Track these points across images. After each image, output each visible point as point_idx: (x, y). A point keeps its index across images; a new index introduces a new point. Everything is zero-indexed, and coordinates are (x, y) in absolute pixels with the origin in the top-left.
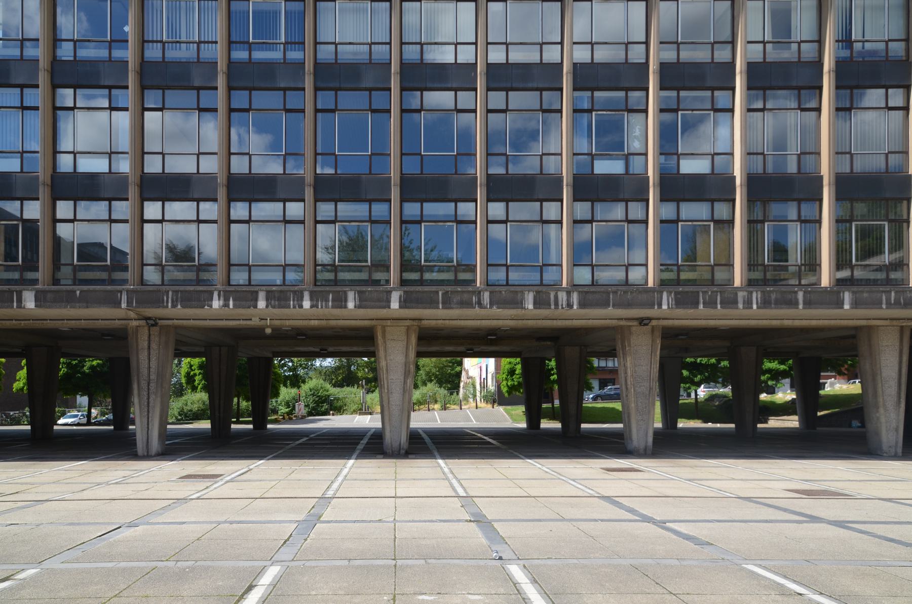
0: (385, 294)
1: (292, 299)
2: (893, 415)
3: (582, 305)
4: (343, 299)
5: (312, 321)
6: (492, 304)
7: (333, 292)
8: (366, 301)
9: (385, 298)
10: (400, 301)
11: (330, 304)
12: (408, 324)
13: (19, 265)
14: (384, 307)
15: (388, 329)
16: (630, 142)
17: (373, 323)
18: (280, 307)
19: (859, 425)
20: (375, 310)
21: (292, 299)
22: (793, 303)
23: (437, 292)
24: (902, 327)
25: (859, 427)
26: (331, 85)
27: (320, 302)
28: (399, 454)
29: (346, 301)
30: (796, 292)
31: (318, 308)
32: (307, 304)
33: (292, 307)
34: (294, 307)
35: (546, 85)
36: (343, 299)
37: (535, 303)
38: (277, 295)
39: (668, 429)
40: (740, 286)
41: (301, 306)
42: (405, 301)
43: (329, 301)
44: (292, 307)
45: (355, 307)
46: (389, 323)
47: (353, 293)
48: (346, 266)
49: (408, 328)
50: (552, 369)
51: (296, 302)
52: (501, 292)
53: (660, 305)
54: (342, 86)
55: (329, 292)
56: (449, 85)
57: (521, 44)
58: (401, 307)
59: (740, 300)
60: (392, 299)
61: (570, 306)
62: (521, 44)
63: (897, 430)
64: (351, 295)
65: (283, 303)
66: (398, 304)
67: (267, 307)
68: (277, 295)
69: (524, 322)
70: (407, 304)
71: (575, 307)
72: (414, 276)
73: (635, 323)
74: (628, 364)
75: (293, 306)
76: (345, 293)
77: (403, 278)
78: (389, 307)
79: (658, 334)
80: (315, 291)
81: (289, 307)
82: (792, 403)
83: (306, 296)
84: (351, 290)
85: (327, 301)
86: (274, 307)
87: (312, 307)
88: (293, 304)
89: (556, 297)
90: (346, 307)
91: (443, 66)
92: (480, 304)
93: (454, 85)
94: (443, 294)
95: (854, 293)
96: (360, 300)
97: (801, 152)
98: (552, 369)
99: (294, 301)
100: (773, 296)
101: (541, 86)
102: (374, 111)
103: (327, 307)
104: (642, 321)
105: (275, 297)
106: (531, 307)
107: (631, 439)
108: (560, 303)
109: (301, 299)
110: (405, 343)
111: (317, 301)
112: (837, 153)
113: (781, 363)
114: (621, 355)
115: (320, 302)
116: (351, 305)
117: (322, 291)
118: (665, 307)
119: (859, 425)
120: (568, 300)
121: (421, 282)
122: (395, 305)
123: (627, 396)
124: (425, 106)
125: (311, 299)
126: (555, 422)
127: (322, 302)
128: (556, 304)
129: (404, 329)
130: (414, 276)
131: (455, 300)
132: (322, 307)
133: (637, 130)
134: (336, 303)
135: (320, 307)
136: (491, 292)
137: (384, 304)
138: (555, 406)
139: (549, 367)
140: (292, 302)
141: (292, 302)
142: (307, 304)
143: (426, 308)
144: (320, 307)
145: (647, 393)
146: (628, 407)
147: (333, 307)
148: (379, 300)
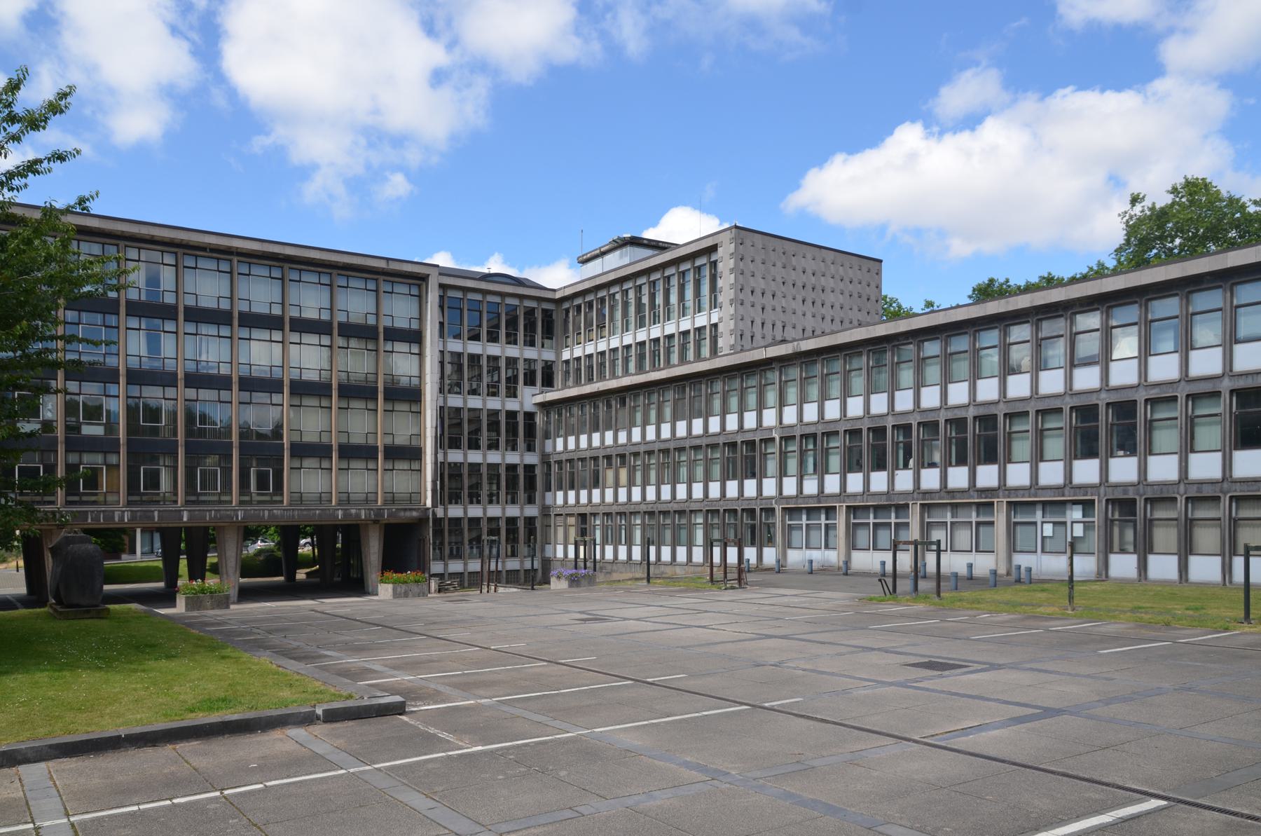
16: (45, 413)
30: (153, 511)
72: (193, 498)
73: (55, 527)
95: (189, 511)
100: (139, 514)
121: (198, 502)
130: (193, 498)
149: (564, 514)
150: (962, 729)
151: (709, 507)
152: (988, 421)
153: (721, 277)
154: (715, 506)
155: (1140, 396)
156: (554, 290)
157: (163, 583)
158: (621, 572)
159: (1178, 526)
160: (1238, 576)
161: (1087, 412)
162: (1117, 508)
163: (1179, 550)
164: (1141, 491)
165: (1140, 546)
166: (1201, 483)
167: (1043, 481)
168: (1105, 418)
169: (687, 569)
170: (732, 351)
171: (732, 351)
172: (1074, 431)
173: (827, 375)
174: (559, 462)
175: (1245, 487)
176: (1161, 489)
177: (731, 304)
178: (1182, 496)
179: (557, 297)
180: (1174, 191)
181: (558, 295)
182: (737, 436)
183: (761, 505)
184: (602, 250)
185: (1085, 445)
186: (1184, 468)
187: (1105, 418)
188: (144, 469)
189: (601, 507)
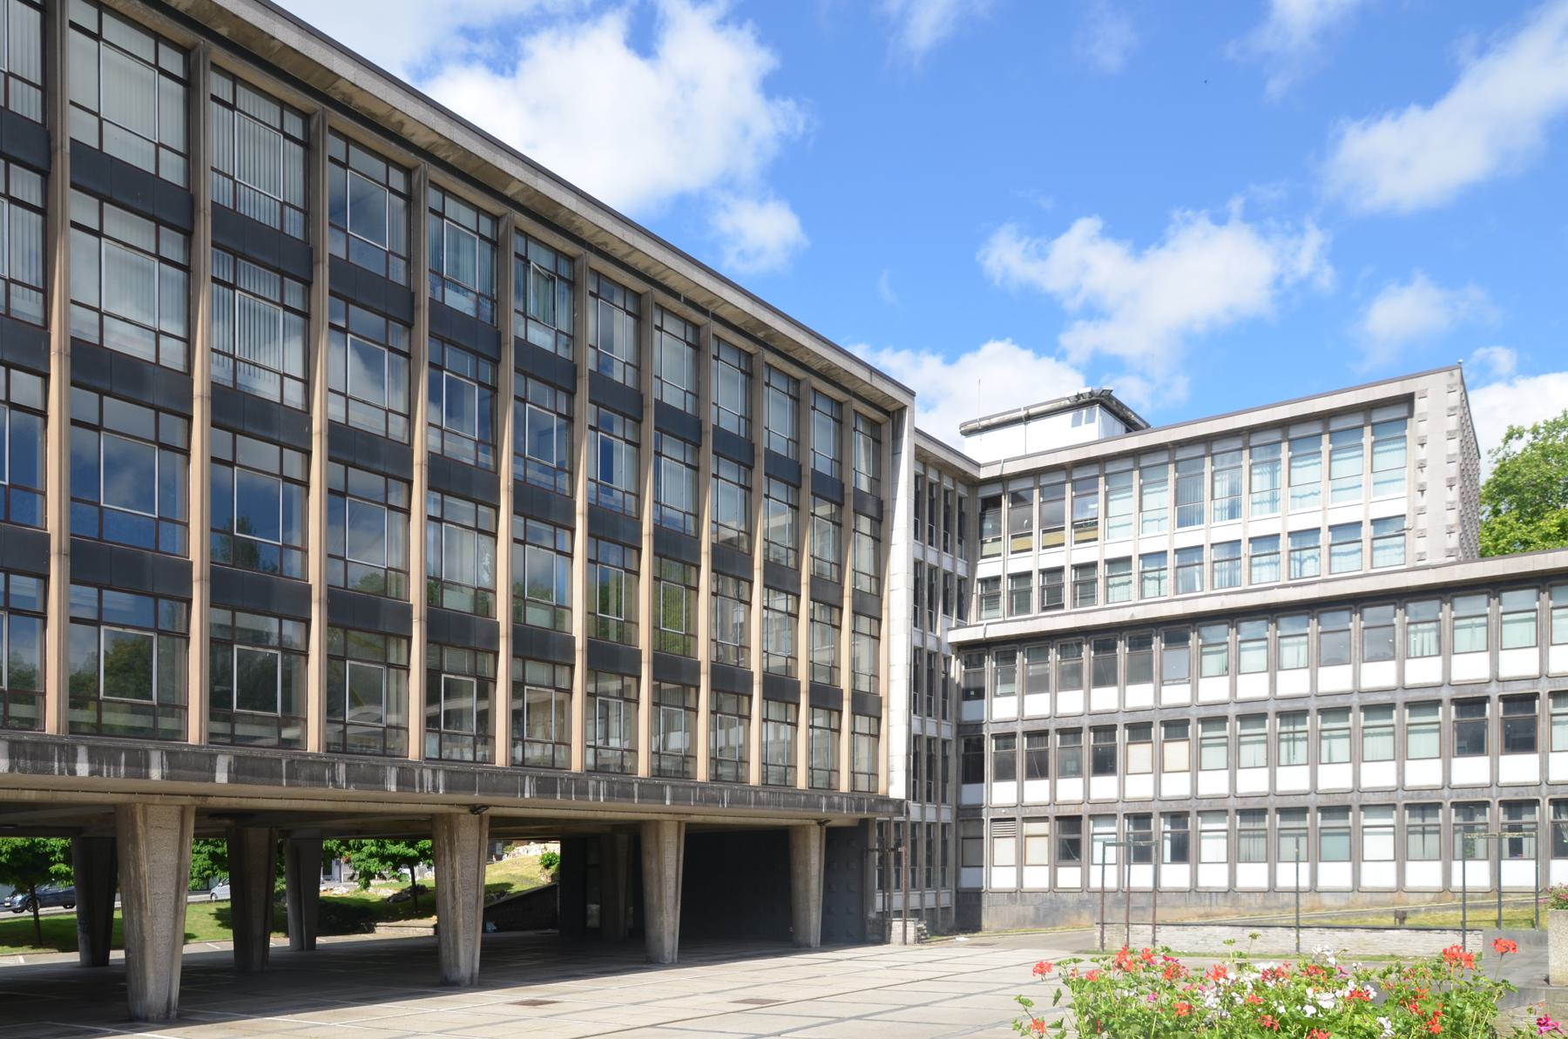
0: (207, 758)
1: (56, 757)
2: (672, 919)
3: (449, 788)
4: (143, 763)
5: (26, 792)
6: (348, 781)
7: (128, 750)
8: (179, 768)
9: (207, 766)
10: (229, 772)
11: (123, 770)
12: (184, 803)
13: (277, 718)
14: (206, 780)
15: (151, 809)
17: (133, 798)
18: (36, 771)
19: (495, 928)
20: (194, 784)
21: (56, 757)
22: (630, 796)
23: (280, 761)
24: (679, 822)
25: (495, 931)
26: (97, 384)
27: (105, 767)
28: (168, 1017)
29: (148, 766)
31: (102, 776)
32: (83, 769)
33: (56, 772)
34: (61, 773)
35: (395, 473)
36: (143, 763)
37: (398, 784)
38: (29, 749)
39: (303, 949)
40: (197, 743)
41: (73, 772)
42: (237, 771)
43: (120, 765)
44: (56, 772)
45: (163, 777)
46: (157, 799)
47: (159, 753)
48: (117, 702)
49: (183, 810)
50: (53, 853)
51: (63, 764)
52: (359, 765)
53: (523, 792)
54: (115, 390)
55: (120, 750)
56: (276, 437)
57: (364, 402)
58: (230, 781)
59: (590, 790)
60: (218, 767)
61: (436, 789)
62: (364, 402)
63: (674, 934)
64: (155, 757)
65: (40, 764)
66: (226, 775)
67: (11, 769)
68: (29, 749)
69: (244, 800)
70: (240, 777)
71: (441, 791)
73: (466, 810)
74: (457, 866)
75: (59, 771)
76: (146, 752)
77: (151, 718)
78: (214, 781)
79: (486, 824)
80: (97, 747)
81: (51, 772)
82: (394, 901)
83: (82, 753)
84: (157, 749)
85: (117, 764)
86: (23, 771)
87: (92, 773)
88: (59, 767)
89: (421, 776)
90: (147, 776)
91: (266, 403)
92: (333, 780)
93: (283, 439)
94: (287, 764)
96: (170, 766)
97: (345, 497)
98: (53, 853)
99: (60, 761)
101: (389, 471)
102: (163, 446)
103: (116, 775)
104: (475, 809)
105: (25, 753)
106: (393, 788)
107: (457, 966)
108: (425, 785)
109: (73, 758)
110: (177, 834)
111: (101, 763)
112: (330, 556)
113: (411, 845)
114: (447, 852)
115: (105, 767)
116: (155, 774)
117: (109, 748)
118: (527, 795)
119: (495, 928)
120: (434, 781)
122: (222, 777)
123: (453, 908)
124: (240, 459)
125: (91, 760)
126: (49, 950)
127: (109, 765)
128: (421, 786)
129: (176, 811)
131: (303, 774)
132: (108, 776)
133: (487, 559)
134: (133, 770)
135: (105, 774)
136: (347, 765)
137: (206, 774)
138: (41, 918)
139: (47, 849)
140: (56, 764)
141: (56, 764)
142: (83, 769)
143: (264, 784)
144: (105, 774)
145: (474, 902)
146: (456, 923)
147: (127, 775)
148: (199, 768)
149: (1400, 804)
150: (696, 994)
151: (1412, 799)
152: (1521, 702)
153: (1422, 445)
154: (1428, 797)
155: (1544, 688)
156: (979, 466)
157: (272, 944)
158: (1174, 907)
159: (1227, 837)
160: (1457, 882)
161: (1471, 705)
162: (1132, 821)
163: (1049, 861)
164: (1494, 794)
165: (1494, 853)
166: (1420, 790)
167: (1028, 799)
168: (1494, 712)
169: (1351, 898)
170: (1452, 559)
171: (1452, 559)
172: (1460, 728)
173: (1280, 637)
174: (1006, 739)
175: (1514, 790)
176: (1419, 794)
177: (1451, 487)
178: (1544, 799)
179: (981, 477)
180: (1494, 473)
181: (984, 474)
182: (1488, 687)
183: (1451, 797)
184: (1032, 411)
185: (1472, 743)
186: (1356, 777)
187: (1494, 712)
188: (276, 711)
189: (1446, 792)
